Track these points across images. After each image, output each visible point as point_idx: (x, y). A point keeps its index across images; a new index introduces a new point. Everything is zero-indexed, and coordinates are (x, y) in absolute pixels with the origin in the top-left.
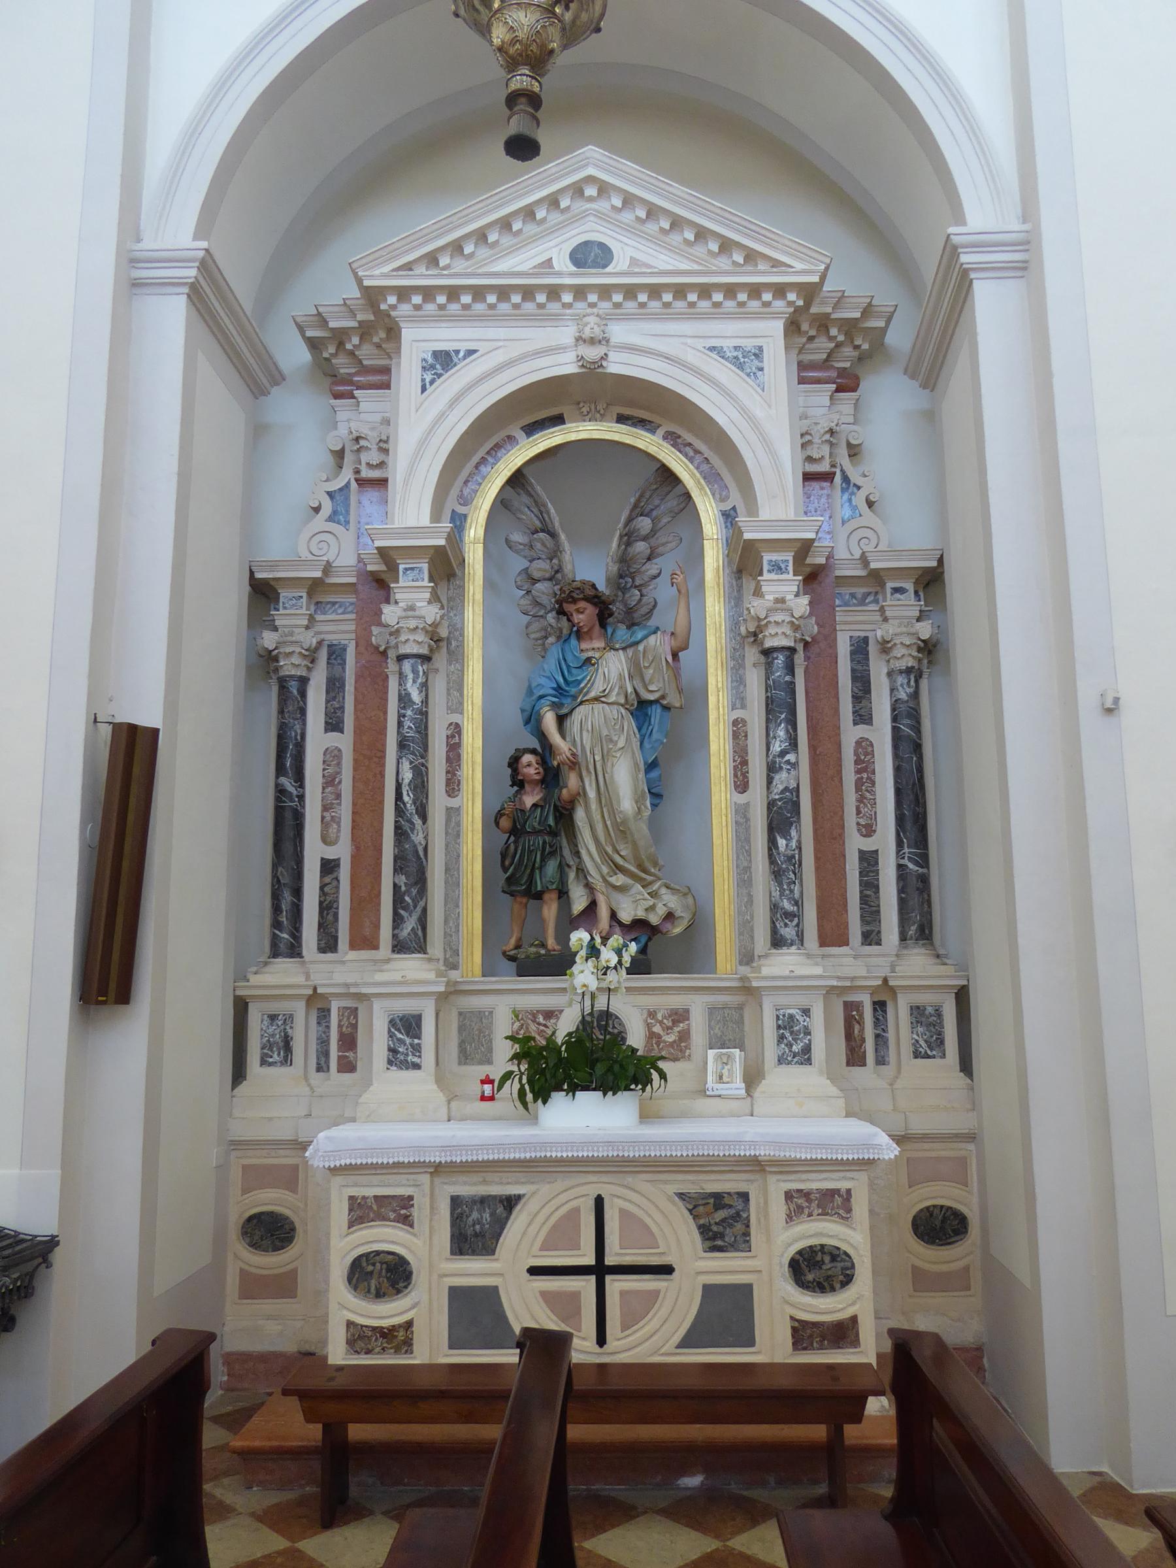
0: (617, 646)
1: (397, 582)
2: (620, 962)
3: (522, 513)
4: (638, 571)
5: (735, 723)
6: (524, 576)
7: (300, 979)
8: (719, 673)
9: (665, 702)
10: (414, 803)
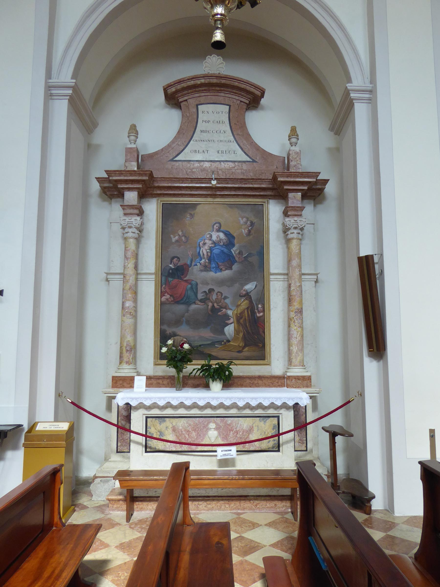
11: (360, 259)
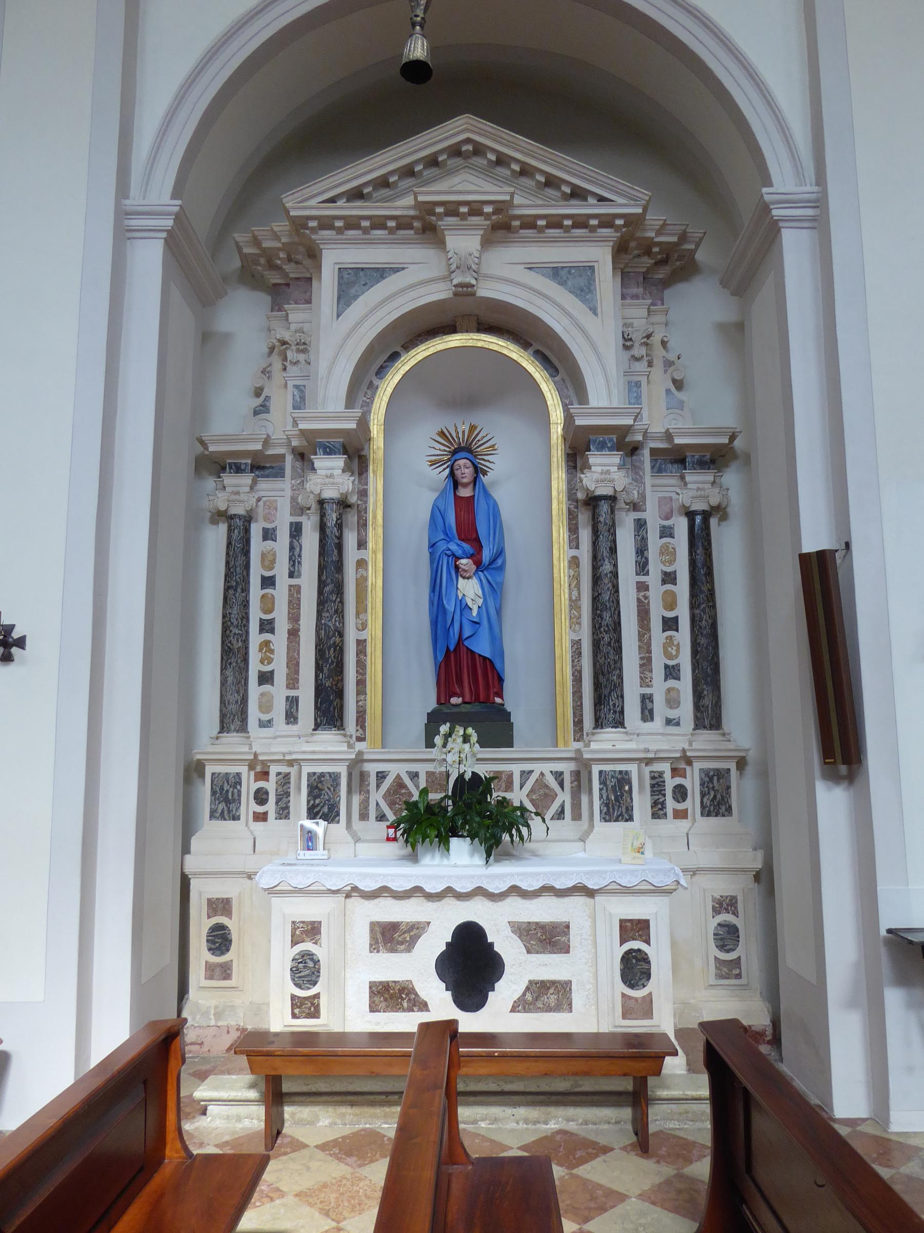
7: (246, 749)
11: (805, 559)
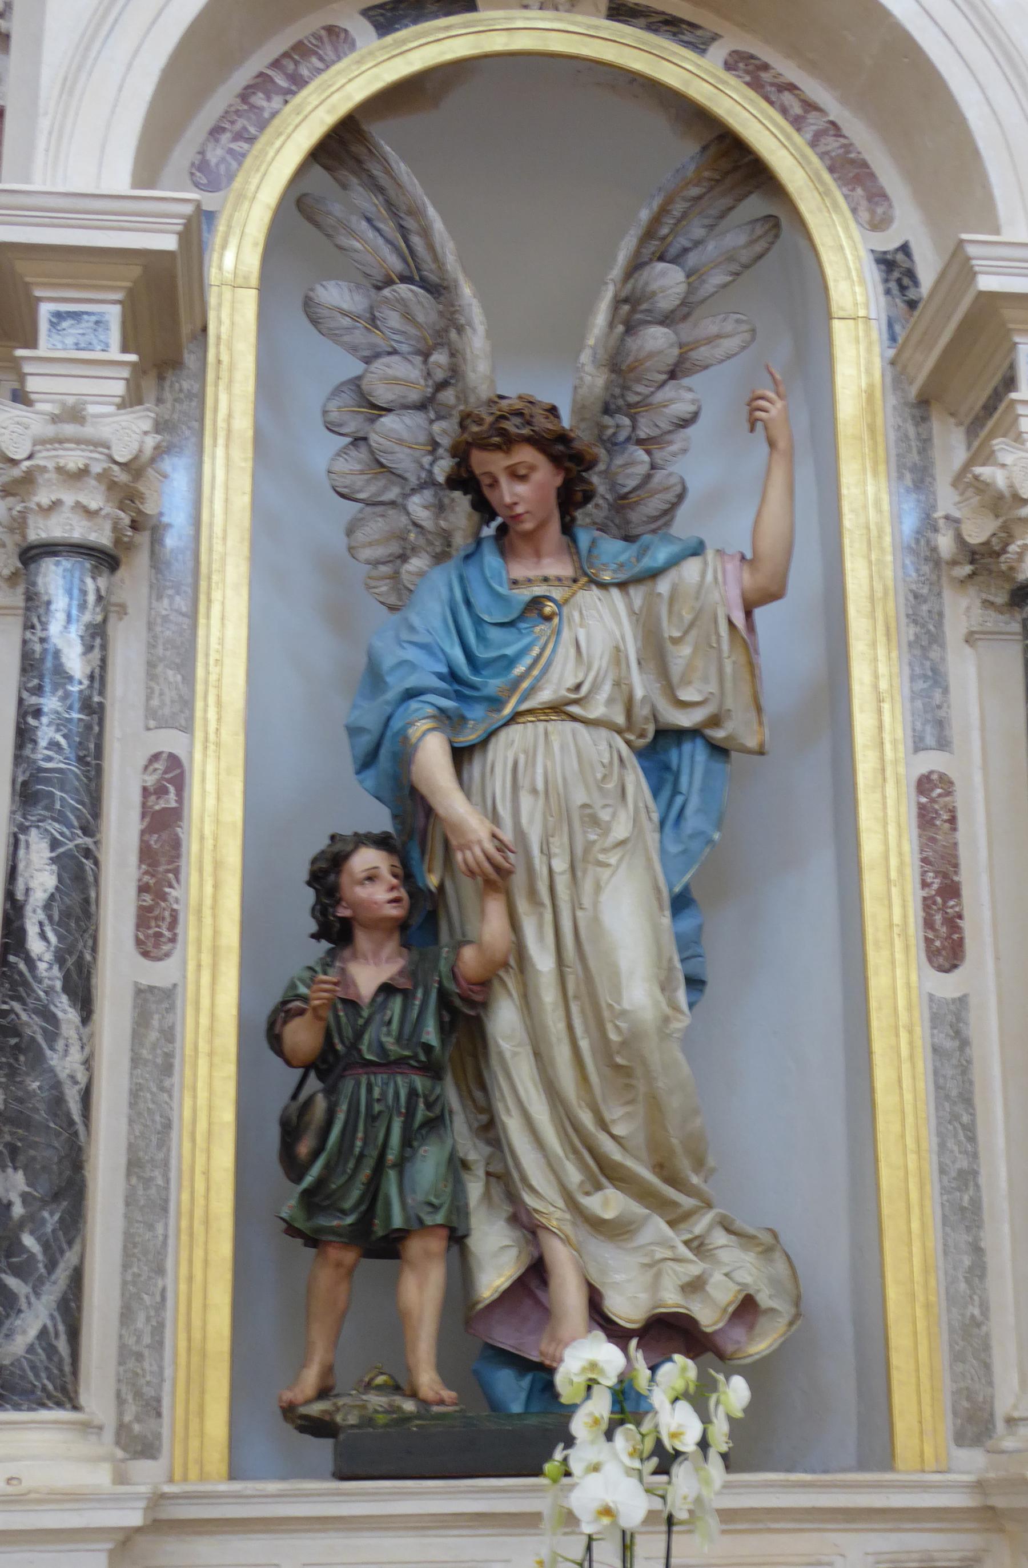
0: (607, 577)
1: (33, 344)
2: (704, 1444)
3: (352, 233)
4: (644, 404)
5: (924, 784)
6: (348, 398)
8: (881, 652)
9: (718, 734)
10: (60, 959)
